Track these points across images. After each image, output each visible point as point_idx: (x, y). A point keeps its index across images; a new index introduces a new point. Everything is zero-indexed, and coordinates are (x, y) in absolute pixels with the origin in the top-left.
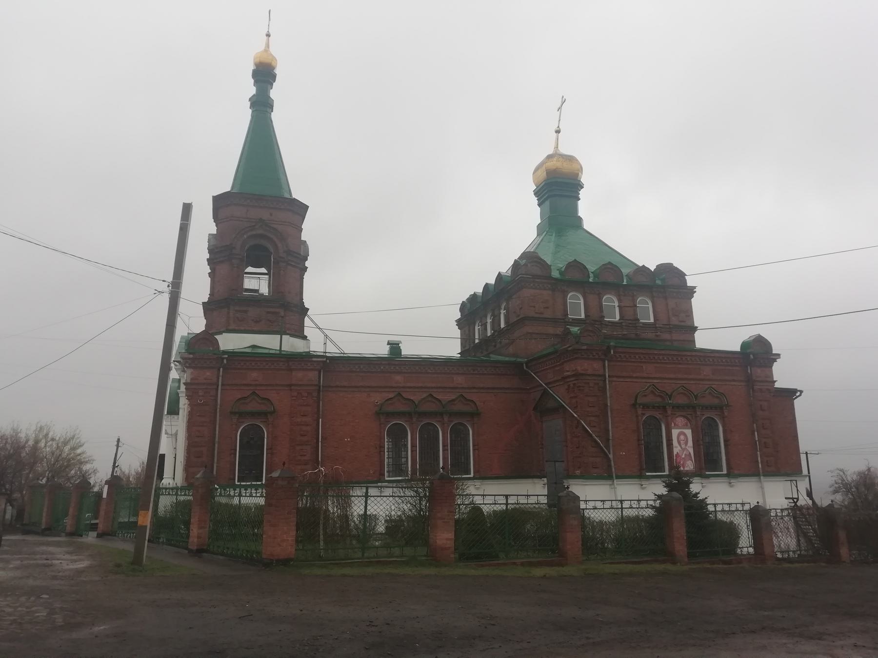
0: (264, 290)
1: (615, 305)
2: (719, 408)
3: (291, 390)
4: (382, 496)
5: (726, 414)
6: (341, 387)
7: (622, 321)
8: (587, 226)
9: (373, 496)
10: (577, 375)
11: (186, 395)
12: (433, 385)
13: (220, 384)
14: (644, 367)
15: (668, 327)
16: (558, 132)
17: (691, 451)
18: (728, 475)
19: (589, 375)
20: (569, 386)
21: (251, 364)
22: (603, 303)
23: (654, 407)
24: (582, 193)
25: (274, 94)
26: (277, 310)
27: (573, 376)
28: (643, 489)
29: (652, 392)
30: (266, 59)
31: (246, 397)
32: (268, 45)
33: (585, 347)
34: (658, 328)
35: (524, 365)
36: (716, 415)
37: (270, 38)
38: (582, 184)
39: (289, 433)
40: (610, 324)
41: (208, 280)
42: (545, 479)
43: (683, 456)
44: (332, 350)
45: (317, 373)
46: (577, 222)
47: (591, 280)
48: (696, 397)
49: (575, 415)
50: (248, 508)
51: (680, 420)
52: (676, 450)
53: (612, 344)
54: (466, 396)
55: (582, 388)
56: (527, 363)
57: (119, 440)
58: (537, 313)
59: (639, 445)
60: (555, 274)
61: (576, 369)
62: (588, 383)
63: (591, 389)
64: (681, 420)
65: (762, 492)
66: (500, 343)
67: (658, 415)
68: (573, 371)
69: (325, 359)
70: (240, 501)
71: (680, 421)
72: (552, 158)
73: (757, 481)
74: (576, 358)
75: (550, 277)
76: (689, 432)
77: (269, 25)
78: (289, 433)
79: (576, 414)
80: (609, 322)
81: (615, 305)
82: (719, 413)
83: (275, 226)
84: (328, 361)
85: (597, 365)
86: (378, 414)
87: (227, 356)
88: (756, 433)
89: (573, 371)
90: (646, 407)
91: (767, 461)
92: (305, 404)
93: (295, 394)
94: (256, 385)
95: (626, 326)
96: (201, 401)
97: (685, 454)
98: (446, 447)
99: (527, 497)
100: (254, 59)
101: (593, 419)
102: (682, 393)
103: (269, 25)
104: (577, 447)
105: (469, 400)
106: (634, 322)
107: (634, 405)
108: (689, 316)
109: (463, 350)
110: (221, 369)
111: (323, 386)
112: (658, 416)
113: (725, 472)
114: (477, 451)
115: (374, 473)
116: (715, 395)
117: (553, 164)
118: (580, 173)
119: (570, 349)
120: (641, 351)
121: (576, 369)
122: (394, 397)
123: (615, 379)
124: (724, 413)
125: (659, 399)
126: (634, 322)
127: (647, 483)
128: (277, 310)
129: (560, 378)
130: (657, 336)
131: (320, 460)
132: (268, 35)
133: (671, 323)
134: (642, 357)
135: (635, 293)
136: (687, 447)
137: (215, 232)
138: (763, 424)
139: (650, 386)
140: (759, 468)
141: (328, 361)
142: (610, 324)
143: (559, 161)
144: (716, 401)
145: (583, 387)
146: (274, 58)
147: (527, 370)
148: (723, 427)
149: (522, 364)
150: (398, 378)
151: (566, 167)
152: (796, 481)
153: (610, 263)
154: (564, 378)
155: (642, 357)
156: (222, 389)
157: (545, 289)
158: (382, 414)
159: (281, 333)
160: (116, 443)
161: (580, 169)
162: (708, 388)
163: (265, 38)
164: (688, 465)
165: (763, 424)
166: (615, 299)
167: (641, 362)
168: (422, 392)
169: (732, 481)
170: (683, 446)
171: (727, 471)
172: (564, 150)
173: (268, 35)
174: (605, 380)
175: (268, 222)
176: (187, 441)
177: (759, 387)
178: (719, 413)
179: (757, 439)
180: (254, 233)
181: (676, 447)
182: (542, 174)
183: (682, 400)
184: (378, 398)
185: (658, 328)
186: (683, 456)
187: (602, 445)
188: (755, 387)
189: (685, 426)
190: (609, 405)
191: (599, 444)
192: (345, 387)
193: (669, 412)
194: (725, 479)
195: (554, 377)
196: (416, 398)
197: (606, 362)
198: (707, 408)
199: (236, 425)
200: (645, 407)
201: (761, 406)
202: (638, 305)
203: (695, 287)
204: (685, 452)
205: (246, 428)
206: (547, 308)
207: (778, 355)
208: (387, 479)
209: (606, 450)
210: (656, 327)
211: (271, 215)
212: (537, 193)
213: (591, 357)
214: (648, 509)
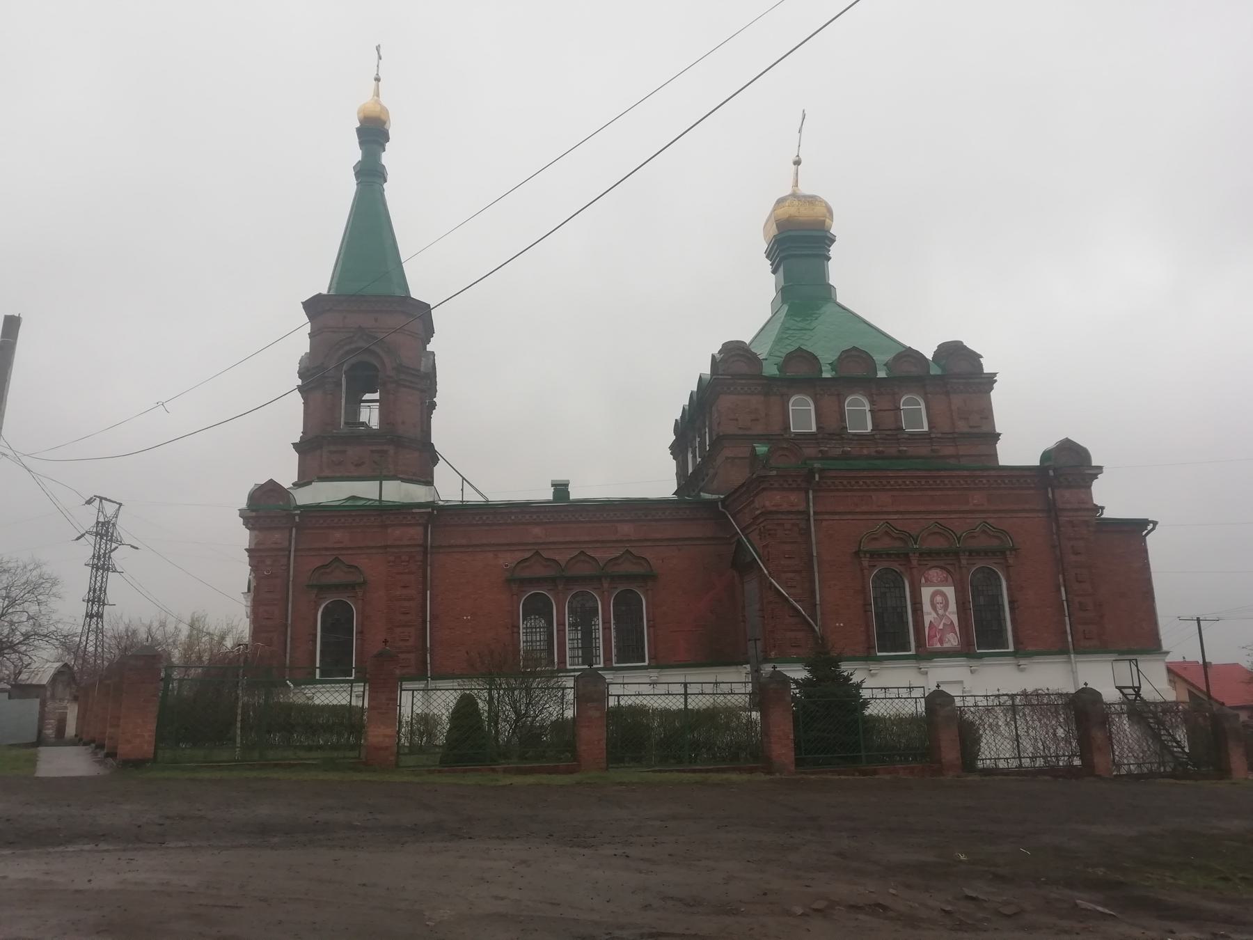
0: (375, 423)
1: (865, 410)
2: (1000, 553)
5: (1011, 561)
6: (456, 546)
7: (874, 432)
8: (841, 298)
9: (627, 695)
10: (766, 513)
12: (587, 539)
13: (293, 549)
17: (955, 619)
18: (1015, 654)
19: (782, 513)
21: (664, 513)
22: (846, 408)
23: (888, 555)
24: (834, 250)
25: (387, 159)
26: (385, 448)
28: (1022, 670)
29: (984, 532)
32: (377, 94)
33: (774, 473)
34: (879, 441)
35: (720, 503)
37: (380, 83)
38: (831, 237)
40: (856, 438)
42: (748, 666)
43: (941, 627)
44: (472, 497)
45: (420, 529)
46: (827, 292)
47: (826, 375)
48: (959, 539)
50: (237, 709)
51: (935, 574)
52: (929, 617)
53: (816, 465)
55: (772, 532)
58: (740, 428)
59: (866, 611)
60: (770, 370)
63: (787, 532)
64: (937, 573)
65: (1074, 678)
67: (898, 566)
69: (430, 510)
70: (619, 701)
71: (936, 574)
72: (783, 202)
73: (1065, 662)
74: (764, 489)
75: (760, 377)
76: (950, 591)
77: (378, 66)
79: (767, 570)
81: (865, 410)
84: (435, 512)
86: (509, 581)
87: (299, 512)
88: (1063, 589)
90: (874, 555)
91: (1084, 631)
93: (392, 558)
94: (339, 549)
95: (880, 439)
96: (268, 571)
97: (944, 624)
99: (883, 690)
100: (358, 113)
102: (935, 533)
103: (378, 66)
106: (895, 433)
107: (857, 553)
108: (986, 418)
110: (294, 530)
111: (431, 546)
112: (897, 567)
113: (1011, 649)
114: (652, 629)
116: (992, 533)
118: (827, 220)
120: (866, 474)
122: (532, 556)
124: (911, 562)
125: (898, 544)
126: (895, 433)
128: (385, 448)
131: (428, 646)
132: (378, 79)
133: (957, 430)
136: (947, 613)
137: (308, 351)
138: (1076, 574)
139: (884, 523)
140: (1068, 642)
141: (435, 512)
142: (856, 438)
143: (793, 206)
144: (995, 543)
145: (775, 530)
146: (385, 110)
147: (723, 510)
148: (1008, 580)
150: (537, 530)
151: (805, 213)
152: (1136, 660)
153: (855, 348)
156: (295, 556)
158: (515, 582)
159: (381, 478)
161: (828, 215)
162: (981, 523)
164: (949, 640)
165: (1076, 574)
169: (1022, 662)
170: (941, 612)
171: (1014, 648)
172: (805, 189)
173: (378, 79)
174: (809, 520)
176: (252, 626)
179: (1064, 598)
180: (353, 346)
181: (953, 613)
182: (773, 231)
183: (938, 543)
184: (508, 559)
185: (934, 440)
186: (941, 627)
187: (804, 613)
188: (1060, 518)
189: (944, 582)
190: (815, 554)
191: (800, 612)
193: (915, 562)
194: (913, 663)
196: (563, 557)
197: (811, 492)
198: (880, 555)
199: (315, 602)
200: (875, 556)
203: (995, 374)
204: (943, 621)
205: (330, 605)
206: (757, 420)
207: (1100, 469)
208: (614, 665)
209: (811, 621)
211: (376, 320)
212: (769, 255)
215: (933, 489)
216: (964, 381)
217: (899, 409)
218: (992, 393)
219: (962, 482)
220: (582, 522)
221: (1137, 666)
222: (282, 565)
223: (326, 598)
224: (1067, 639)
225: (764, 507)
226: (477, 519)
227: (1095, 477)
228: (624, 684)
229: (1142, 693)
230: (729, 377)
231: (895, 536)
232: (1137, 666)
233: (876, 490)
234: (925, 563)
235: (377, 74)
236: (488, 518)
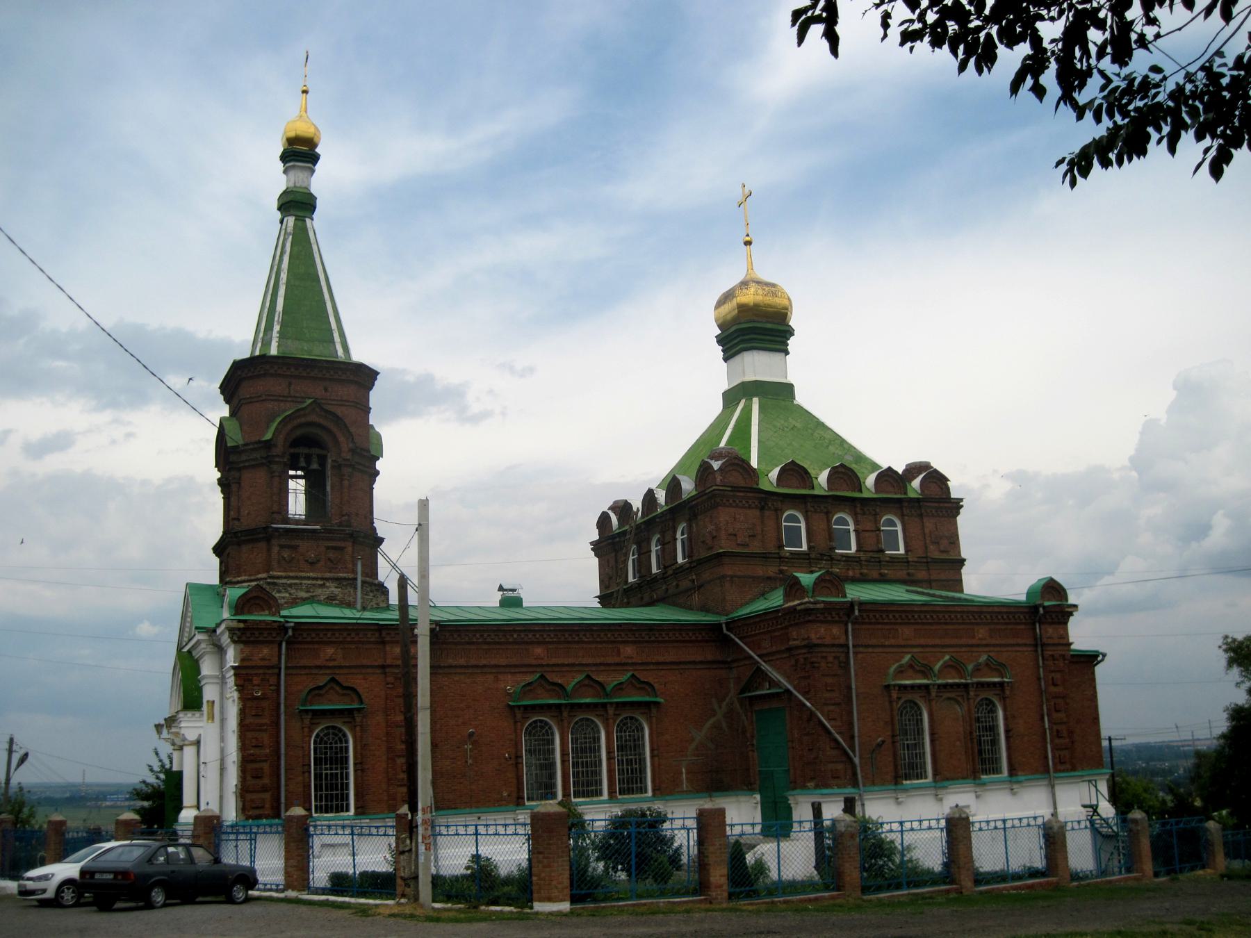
3: (385, 673)
6: (456, 667)
10: (810, 647)
11: (236, 685)
14: (900, 630)
15: (925, 560)
20: (797, 661)
27: (805, 646)
31: (319, 688)
35: (724, 625)
39: (384, 739)
41: (218, 499)
49: (808, 704)
54: (638, 676)
55: (817, 665)
56: (727, 624)
57: (11, 741)
61: (808, 637)
62: (825, 658)
63: (830, 665)
66: (677, 586)
68: (803, 639)
78: (384, 739)
80: (842, 555)
82: (998, 692)
83: (339, 411)
85: (836, 630)
89: (803, 639)
95: (866, 561)
98: (612, 754)
101: (831, 708)
104: (809, 750)
105: (644, 682)
110: (284, 645)
115: (509, 796)
117: (749, 297)
119: (799, 608)
121: (808, 637)
123: (861, 649)
127: (904, 795)
129: (783, 648)
130: (908, 574)
134: (897, 615)
135: (878, 510)
138: (1055, 704)
145: (819, 663)
148: (1005, 710)
149: (720, 625)
154: (789, 649)
155: (897, 615)
156: (286, 675)
157: (750, 507)
160: (7, 746)
167: (895, 624)
169: (1015, 786)
175: (323, 401)
176: (240, 754)
178: (998, 692)
184: (511, 684)
192: (462, 667)
195: (772, 646)
199: (309, 728)
201: (1053, 678)
202: (882, 528)
203: (961, 500)
206: (754, 536)
210: (908, 562)
211: (326, 390)
213: (830, 619)
216: (936, 505)
217: (879, 530)
218: (958, 518)
219: (971, 617)
220: (586, 643)
221: (1096, 787)
222: (271, 685)
223: (318, 723)
225: (808, 638)
226: (478, 636)
227: (1071, 614)
228: (456, 826)
229: (1099, 810)
230: (729, 489)
231: (918, 668)
232: (1096, 787)
233: (901, 624)
236: (489, 635)
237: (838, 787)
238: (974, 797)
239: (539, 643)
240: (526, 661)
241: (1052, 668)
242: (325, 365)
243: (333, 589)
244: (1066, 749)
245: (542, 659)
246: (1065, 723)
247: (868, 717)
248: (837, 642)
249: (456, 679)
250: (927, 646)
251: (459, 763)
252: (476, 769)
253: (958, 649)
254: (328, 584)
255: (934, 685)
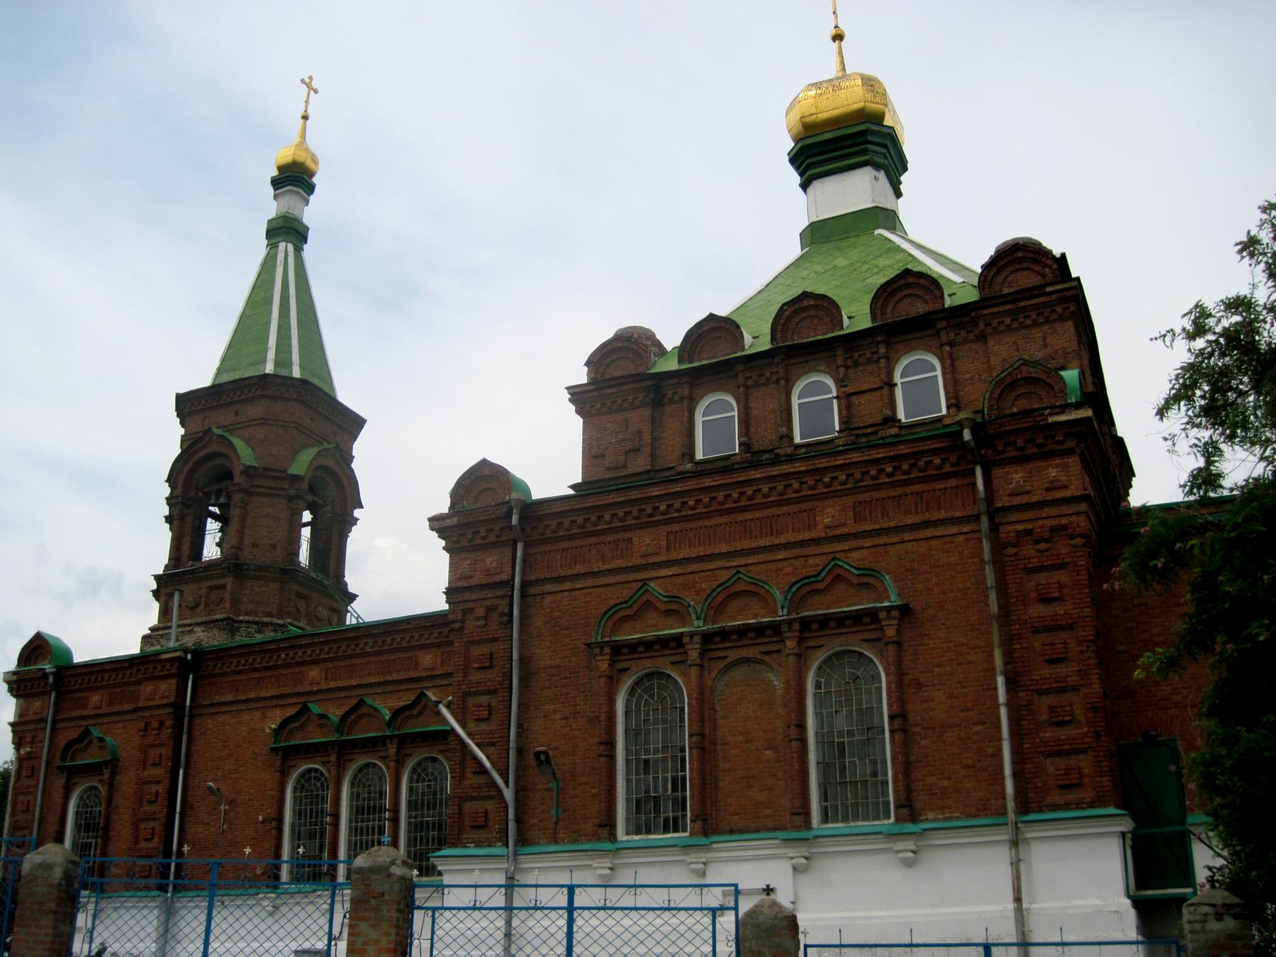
4: (675, 909)
6: (220, 704)
16: (838, 37)
30: (301, 157)
36: (866, 641)
37: (308, 122)
58: (608, 469)
92: (157, 742)
109: (454, 585)
163: (301, 121)
166: (831, 383)
168: (405, 690)
173: (305, 118)
177: (1020, 527)
211: (237, 414)
214: (95, 934)
215: (744, 509)
224: (1004, 789)
234: (721, 654)
235: (306, 111)
237: (477, 846)
238: (790, 871)
239: (316, 662)
240: (300, 689)
241: (1035, 562)
242: (230, 387)
243: (201, 634)
244: (1078, 752)
245: (318, 683)
246: (1075, 689)
247: (555, 712)
248: (497, 579)
249: (221, 720)
250: (688, 560)
251: (213, 829)
252: (230, 837)
253: (768, 557)
254: (195, 629)
255: (692, 635)
